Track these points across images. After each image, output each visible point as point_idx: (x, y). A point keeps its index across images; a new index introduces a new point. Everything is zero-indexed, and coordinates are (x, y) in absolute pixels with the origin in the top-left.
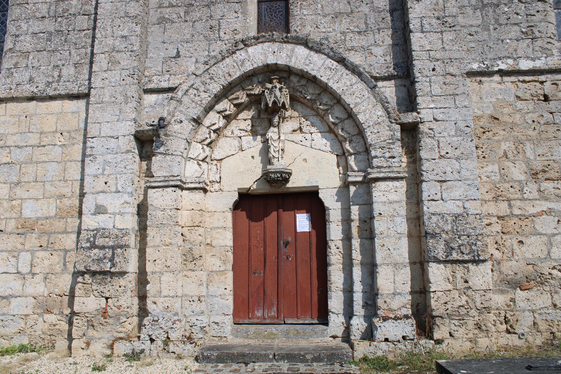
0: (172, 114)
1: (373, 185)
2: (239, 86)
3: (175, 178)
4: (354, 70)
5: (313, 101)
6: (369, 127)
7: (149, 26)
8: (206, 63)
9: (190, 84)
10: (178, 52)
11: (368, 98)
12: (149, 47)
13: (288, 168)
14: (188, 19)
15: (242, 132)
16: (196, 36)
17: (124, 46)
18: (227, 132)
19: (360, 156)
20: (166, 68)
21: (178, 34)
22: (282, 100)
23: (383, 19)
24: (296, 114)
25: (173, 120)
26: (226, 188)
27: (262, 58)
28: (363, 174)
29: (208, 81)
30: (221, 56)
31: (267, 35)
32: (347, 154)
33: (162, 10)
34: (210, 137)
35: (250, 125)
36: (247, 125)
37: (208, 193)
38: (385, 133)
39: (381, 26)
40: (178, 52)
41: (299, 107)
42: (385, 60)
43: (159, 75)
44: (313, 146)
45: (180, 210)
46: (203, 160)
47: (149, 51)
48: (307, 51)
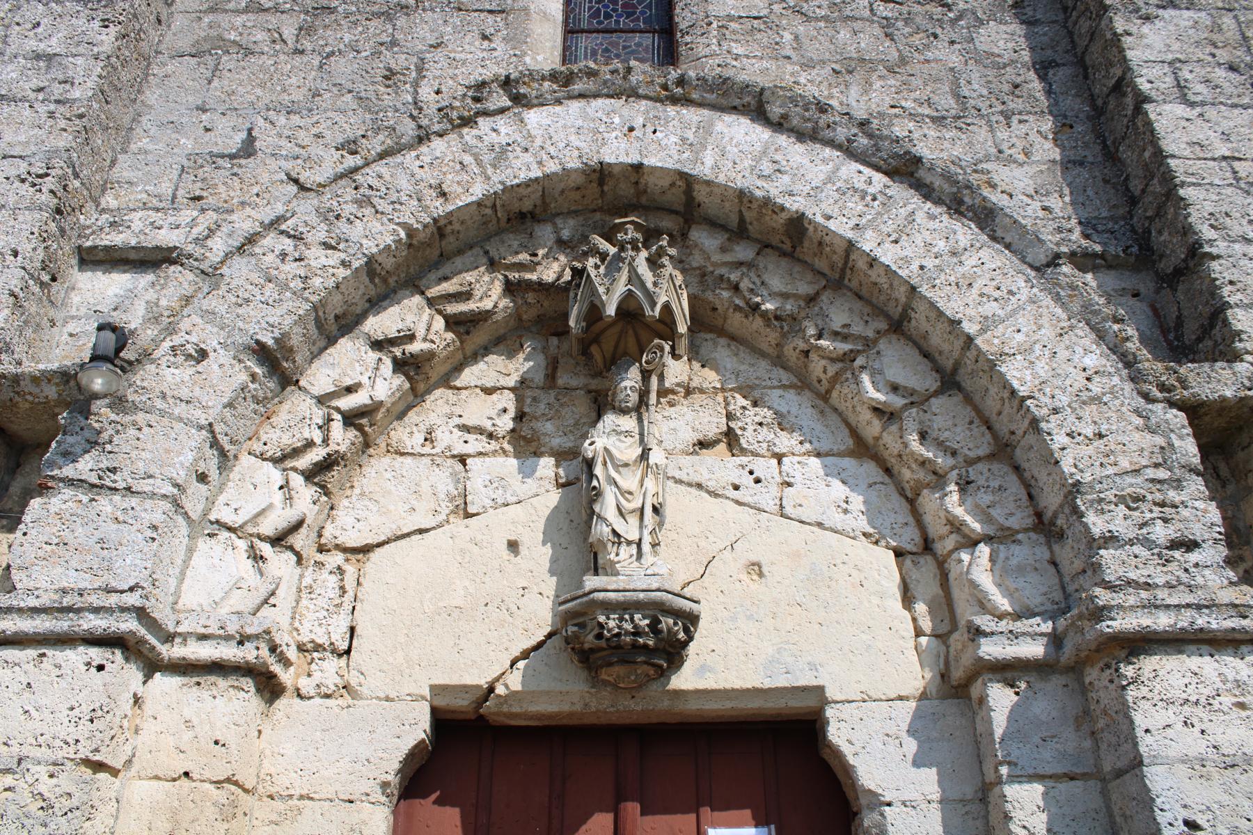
0: (166, 320)
1: (1128, 671)
2: (477, 250)
3: (113, 600)
4: (961, 202)
5: (785, 323)
6: (1056, 411)
7: (160, 58)
8: (350, 146)
9: (267, 215)
10: (250, 139)
11: (1032, 301)
12: (144, 119)
13: (687, 592)
14: (308, 46)
15: (471, 437)
16: (327, 96)
17: (35, 83)
18: (407, 434)
19: (1016, 549)
20: (191, 186)
21: (262, 85)
22: (662, 300)
23: (1016, 86)
24: (710, 378)
25: (167, 344)
26: (372, 684)
27: (582, 145)
28: (1047, 627)
29: (349, 209)
30: (413, 125)
31: (607, 68)
32: (945, 545)
33: (220, 17)
34: (326, 441)
35: (512, 413)
36: (497, 412)
37: (281, 703)
38: (1134, 445)
39: (1011, 105)
40: (250, 139)
41: (722, 352)
42: (1045, 209)
43: (158, 210)
44: (789, 510)
45: (114, 772)
46: (278, 540)
47: (139, 130)
48: (761, 134)
